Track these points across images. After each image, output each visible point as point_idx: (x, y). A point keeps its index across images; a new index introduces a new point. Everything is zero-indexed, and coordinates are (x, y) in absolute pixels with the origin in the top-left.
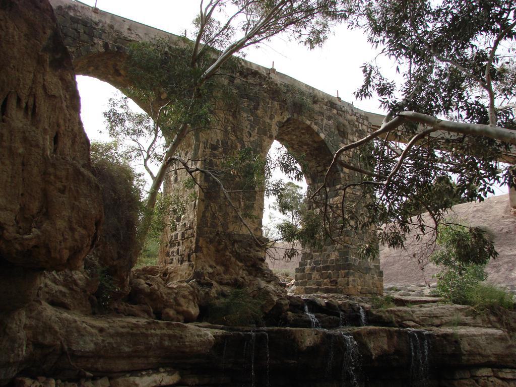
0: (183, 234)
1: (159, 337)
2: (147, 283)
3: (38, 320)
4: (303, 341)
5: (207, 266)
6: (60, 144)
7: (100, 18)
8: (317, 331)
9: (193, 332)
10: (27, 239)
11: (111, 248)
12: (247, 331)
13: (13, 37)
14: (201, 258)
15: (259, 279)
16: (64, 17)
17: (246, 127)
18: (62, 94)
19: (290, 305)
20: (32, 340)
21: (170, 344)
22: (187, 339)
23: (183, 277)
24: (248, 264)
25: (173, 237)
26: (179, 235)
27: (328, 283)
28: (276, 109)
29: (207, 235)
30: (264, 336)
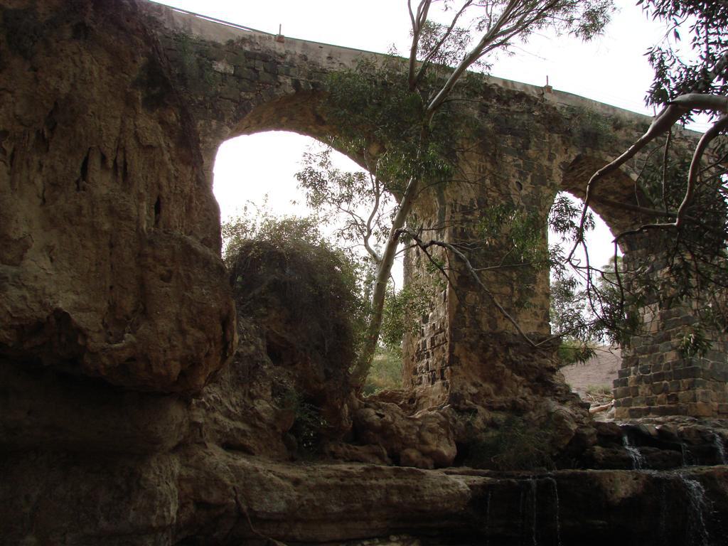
0: (433, 339)
1: (383, 490)
2: (377, 414)
3: (197, 468)
4: (613, 489)
5: (468, 384)
6: (164, 213)
7: (287, 49)
8: (637, 473)
9: (434, 480)
10: (117, 349)
11: (315, 365)
12: (524, 477)
13: (91, 73)
14: (458, 374)
15: (549, 399)
16: (236, 54)
17: (514, 176)
18: (163, 143)
19: (599, 435)
20: (192, 497)
21: (401, 500)
22: (427, 492)
23: (436, 402)
24: (531, 378)
25: (421, 346)
26: (427, 342)
27: (663, 399)
28: (557, 146)
29: (466, 339)
30: (551, 482)
